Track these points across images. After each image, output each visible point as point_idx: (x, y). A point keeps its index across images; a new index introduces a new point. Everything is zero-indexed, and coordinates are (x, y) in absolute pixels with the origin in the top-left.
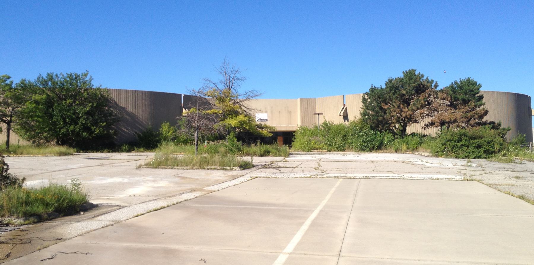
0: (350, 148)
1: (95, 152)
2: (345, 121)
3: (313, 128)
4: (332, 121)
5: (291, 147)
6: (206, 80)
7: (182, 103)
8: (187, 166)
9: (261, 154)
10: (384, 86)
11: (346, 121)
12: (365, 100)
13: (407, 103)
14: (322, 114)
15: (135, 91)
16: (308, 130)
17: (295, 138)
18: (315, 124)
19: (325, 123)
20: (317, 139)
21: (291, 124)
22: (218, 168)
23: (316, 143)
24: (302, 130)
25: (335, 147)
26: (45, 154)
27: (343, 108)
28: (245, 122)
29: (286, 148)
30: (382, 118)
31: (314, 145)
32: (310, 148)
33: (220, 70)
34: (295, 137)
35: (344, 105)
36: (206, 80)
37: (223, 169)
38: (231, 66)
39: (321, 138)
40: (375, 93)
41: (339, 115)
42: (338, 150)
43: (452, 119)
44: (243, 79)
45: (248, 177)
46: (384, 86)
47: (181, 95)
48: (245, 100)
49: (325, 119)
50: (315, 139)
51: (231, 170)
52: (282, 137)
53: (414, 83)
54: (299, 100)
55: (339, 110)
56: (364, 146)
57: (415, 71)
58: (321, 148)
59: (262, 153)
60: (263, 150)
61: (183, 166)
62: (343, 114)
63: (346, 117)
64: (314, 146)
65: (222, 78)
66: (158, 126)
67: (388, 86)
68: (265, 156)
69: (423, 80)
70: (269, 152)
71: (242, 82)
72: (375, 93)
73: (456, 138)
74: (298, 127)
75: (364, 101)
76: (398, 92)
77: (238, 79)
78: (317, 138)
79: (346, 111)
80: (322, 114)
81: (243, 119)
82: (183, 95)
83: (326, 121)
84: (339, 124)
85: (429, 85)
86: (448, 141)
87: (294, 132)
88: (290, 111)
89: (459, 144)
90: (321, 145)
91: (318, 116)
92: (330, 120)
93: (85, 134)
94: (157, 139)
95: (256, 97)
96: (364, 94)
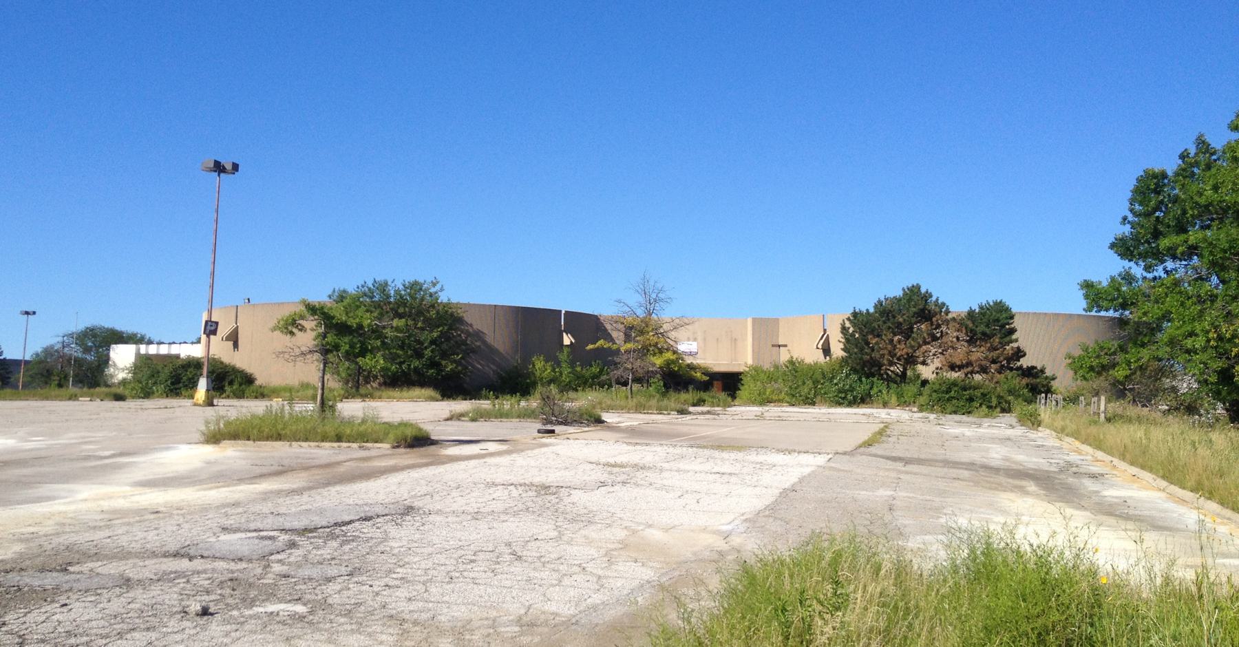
1: (445, 398)
5: (735, 398)
6: (619, 301)
7: (562, 323)
8: (622, 410)
9: (693, 403)
10: (872, 310)
12: (845, 330)
13: (908, 334)
14: (786, 346)
15: (495, 306)
16: (763, 371)
17: (743, 385)
19: (791, 362)
20: (776, 386)
21: (736, 361)
22: (655, 412)
24: (753, 371)
26: (412, 398)
28: (673, 362)
29: (723, 396)
30: (868, 357)
32: (764, 400)
33: (637, 288)
34: (742, 382)
35: (825, 331)
36: (619, 301)
37: (661, 414)
38: (652, 283)
40: (858, 320)
43: (964, 362)
44: (669, 300)
45: (688, 418)
46: (872, 310)
47: (561, 311)
48: (672, 330)
51: (669, 414)
53: (914, 307)
55: (816, 338)
56: (841, 398)
57: (918, 287)
59: (695, 402)
60: (696, 398)
61: (618, 410)
62: (822, 345)
63: (826, 351)
65: (641, 299)
66: (527, 359)
67: (878, 310)
68: (699, 405)
69: (931, 301)
70: (704, 401)
71: (668, 305)
72: (858, 320)
73: (944, 388)
75: (844, 331)
76: (892, 320)
77: (662, 300)
80: (786, 346)
81: (671, 357)
82: (563, 312)
83: (792, 357)
84: (812, 363)
85: (937, 310)
86: (935, 391)
87: (740, 374)
89: (947, 396)
90: (781, 397)
93: (431, 371)
94: (528, 381)
95: (687, 326)
96: (843, 321)
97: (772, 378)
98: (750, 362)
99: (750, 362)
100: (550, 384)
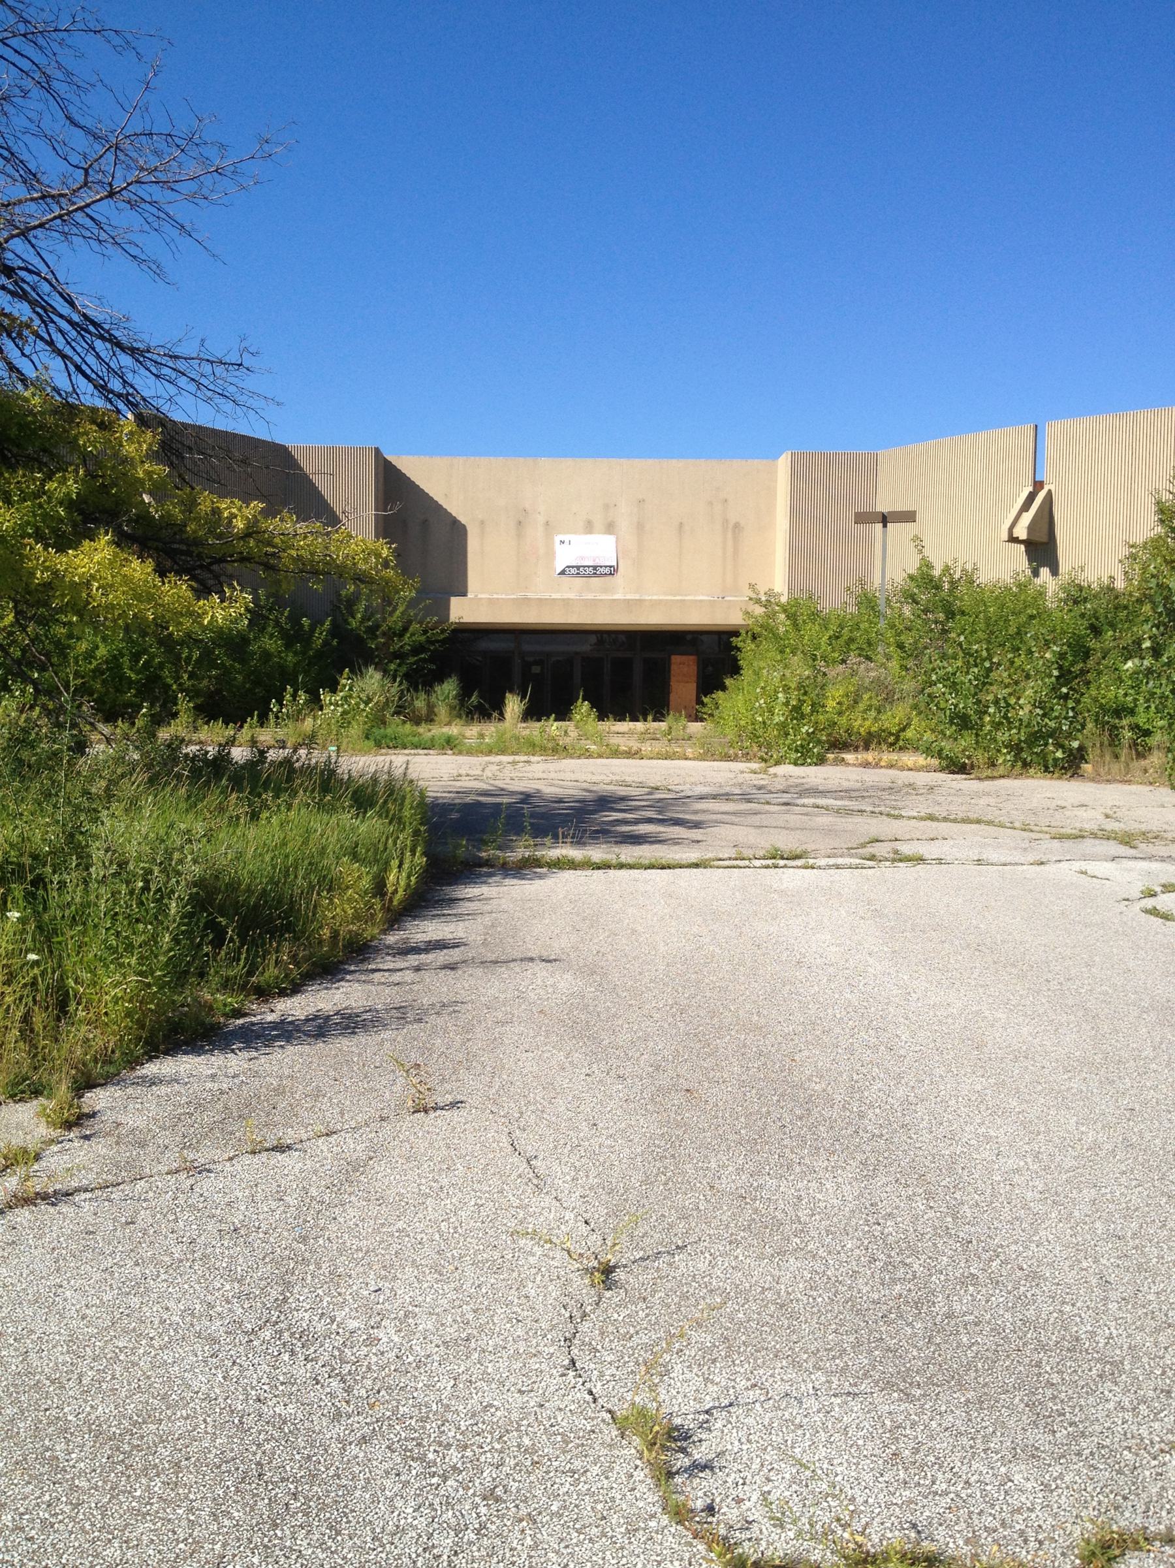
0: (1124, 753)
2: (1036, 573)
3: (851, 609)
4: (969, 567)
11: (1045, 572)
14: (908, 517)
16: (814, 615)
18: (861, 581)
19: (925, 579)
20: (869, 672)
23: (856, 702)
25: (1002, 736)
27: (1031, 498)
31: (840, 713)
35: (1038, 485)
39: (894, 665)
41: (1005, 536)
42: (1026, 765)
49: (926, 552)
50: (854, 673)
52: (692, 657)
54: (783, 463)
58: (894, 740)
62: (1031, 528)
64: (843, 721)
74: (758, 601)
78: (868, 670)
79: (1046, 517)
80: (908, 517)
83: (929, 566)
88: (737, 526)
90: (892, 719)
91: (885, 534)
92: (955, 560)
97: (852, 640)
98: (778, 583)
99: (778, 583)
100: (440, 677)
